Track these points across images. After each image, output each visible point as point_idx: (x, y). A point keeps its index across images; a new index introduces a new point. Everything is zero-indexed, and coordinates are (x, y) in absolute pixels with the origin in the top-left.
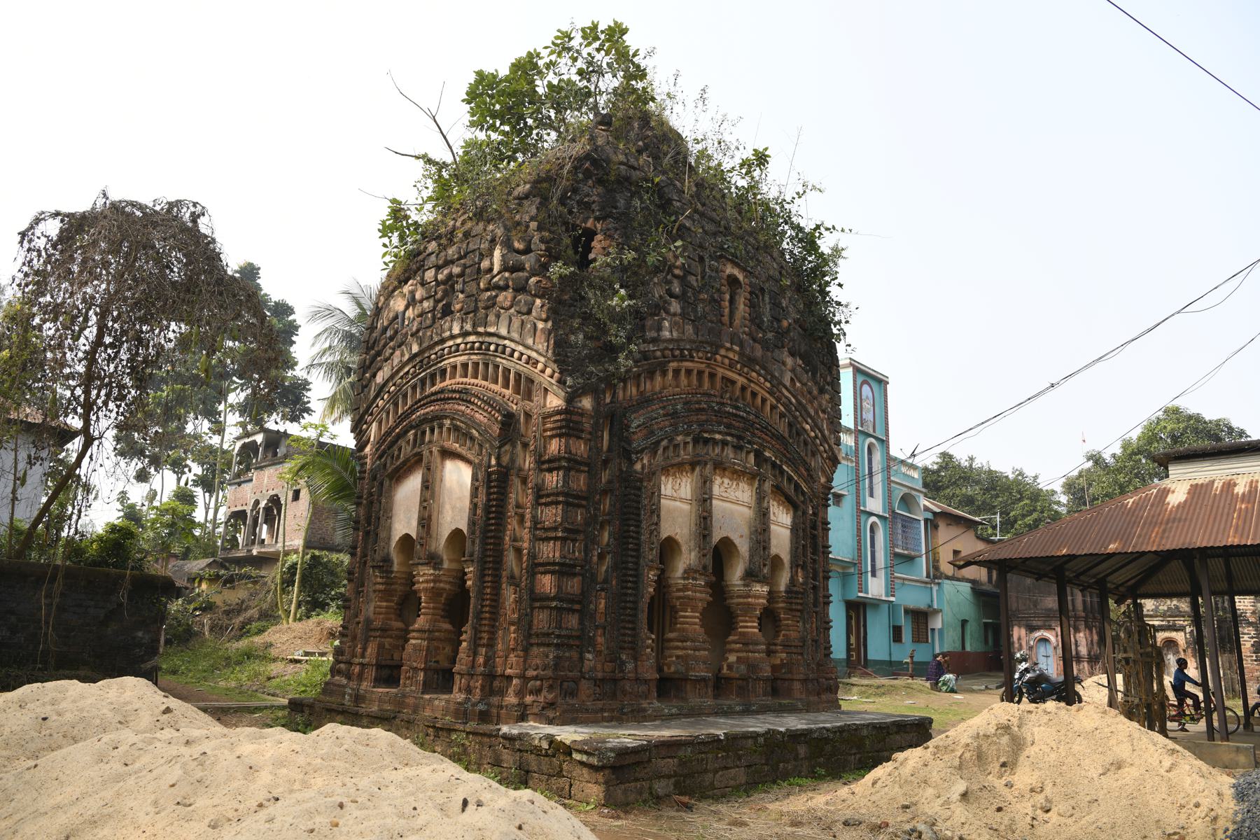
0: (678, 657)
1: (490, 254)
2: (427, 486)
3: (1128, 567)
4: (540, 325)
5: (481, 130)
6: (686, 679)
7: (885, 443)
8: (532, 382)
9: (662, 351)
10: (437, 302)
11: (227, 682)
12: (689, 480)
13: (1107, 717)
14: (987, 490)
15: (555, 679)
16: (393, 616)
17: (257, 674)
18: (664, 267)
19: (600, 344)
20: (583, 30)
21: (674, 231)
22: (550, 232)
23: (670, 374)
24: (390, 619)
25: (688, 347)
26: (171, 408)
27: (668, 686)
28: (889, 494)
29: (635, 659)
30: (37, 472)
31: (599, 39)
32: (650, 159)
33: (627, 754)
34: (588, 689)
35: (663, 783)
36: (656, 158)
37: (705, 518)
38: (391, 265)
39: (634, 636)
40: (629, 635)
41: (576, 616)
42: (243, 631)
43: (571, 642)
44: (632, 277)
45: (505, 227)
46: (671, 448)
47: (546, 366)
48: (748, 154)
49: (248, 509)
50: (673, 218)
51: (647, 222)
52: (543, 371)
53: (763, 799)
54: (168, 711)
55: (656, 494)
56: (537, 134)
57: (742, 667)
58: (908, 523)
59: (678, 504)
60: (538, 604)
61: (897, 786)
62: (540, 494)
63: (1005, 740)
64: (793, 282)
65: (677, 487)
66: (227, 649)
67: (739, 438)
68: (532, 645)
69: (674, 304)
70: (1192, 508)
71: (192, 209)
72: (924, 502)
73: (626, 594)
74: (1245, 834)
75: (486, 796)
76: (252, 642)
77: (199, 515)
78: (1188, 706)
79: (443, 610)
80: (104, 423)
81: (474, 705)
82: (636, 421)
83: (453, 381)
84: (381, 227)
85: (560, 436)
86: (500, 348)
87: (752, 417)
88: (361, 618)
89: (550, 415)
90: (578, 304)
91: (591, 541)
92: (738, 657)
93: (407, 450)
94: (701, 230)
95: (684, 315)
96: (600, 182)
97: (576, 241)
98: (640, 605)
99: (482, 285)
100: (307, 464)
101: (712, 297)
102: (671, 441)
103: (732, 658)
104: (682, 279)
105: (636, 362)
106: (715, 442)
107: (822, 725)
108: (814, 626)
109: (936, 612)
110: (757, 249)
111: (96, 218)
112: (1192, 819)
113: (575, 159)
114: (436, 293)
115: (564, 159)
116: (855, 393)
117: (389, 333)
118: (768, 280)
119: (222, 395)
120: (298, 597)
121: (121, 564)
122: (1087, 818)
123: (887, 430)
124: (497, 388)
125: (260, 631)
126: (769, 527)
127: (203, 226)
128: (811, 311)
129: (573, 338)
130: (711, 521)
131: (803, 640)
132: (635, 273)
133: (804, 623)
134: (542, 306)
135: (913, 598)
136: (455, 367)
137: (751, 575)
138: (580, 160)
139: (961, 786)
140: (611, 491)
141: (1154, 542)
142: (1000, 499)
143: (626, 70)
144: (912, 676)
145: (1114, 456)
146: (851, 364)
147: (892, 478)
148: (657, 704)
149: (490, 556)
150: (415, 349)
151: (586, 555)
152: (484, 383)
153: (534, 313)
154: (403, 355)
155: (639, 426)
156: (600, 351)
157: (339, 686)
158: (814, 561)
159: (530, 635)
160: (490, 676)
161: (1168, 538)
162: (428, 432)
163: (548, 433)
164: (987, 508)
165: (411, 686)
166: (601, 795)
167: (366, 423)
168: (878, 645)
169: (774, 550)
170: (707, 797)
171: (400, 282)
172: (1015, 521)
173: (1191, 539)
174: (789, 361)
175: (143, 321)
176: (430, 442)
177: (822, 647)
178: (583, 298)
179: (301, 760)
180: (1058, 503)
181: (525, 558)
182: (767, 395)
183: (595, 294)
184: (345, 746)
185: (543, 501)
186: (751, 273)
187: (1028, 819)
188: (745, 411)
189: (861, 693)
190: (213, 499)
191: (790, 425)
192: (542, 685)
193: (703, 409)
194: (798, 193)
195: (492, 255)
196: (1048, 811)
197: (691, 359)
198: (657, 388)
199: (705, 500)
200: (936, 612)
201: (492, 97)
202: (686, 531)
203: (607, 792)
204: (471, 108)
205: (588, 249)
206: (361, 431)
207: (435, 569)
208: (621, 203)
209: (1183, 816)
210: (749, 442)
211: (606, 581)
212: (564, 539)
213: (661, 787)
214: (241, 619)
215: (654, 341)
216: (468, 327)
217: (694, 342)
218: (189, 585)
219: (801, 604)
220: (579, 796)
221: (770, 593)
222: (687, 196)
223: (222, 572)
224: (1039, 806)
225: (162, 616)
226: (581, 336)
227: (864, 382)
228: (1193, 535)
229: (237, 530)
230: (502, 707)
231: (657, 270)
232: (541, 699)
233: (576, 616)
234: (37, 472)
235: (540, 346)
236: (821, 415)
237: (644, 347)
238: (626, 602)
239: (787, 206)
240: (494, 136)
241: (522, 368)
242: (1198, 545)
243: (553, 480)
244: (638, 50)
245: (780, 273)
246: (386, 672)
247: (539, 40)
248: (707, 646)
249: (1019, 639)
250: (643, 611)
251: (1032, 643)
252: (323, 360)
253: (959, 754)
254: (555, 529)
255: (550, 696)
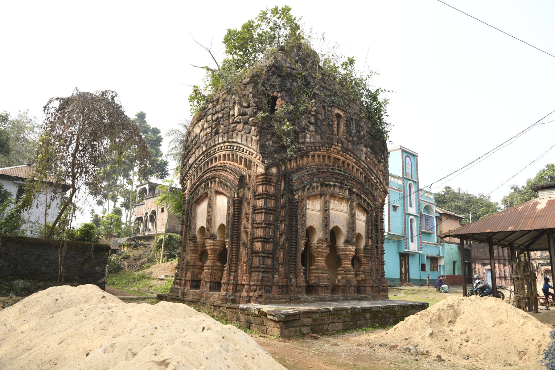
0: (315, 277)
1: (233, 108)
2: (210, 206)
3: (523, 237)
4: (254, 138)
5: (231, 54)
6: (318, 286)
7: (416, 183)
8: (251, 162)
9: (307, 147)
10: (213, 129)
11: (134, 288)
12: (319, 202)
13: (497, 302)
14: (467, 203)
15: (262, 286)
16: (197, 260)
17: (146, 285)
18: (307, 111)
19: (279, 145)
20: (272, 10)
21: (312, 96)
22: (258, 98)
23: (310, 157)
24: (197, 262)
25: (318, 145)
26: (110, 175)
27: (310, 289)
28: (419, 205)
29: (296, 277)
30: (54, 203)
31: (279, 13)
32: (301, 65)
33: (289, 316)
34: (276, 289)
35: (306, 328)
36: (304, 64)
37: (326, 218)
38: (194, 114)
39: (295, 268)
40: (293, 268)
41: (271, 259)
42: (141, 267)
43: (269, 270)
44: (293, 117)
45: (239, 97)
46: (311, 189)
47: (256, 155)
48: (346, 60)
49: (143, 216)
50: (311, 90)
51: (300, 92)
52: (255, 158)
53: (349, 336)
54: (103, 297)
55: (304, 208)
56: (254, 55)
57: (344, 281)
58: (428, 218)
59: (314, 212)
60: (254, 255)
61: (404, 330)
62: (255, 209)
63: (451, 311)
64: (366, 115)
65: (314, 205)
66: (134, 275)
67: (341, 183)
68: (252, 271)
69: (311, 127)
70: (547, 211)
71: (112, 94)
72: (435, 209)
73: (292, 250)
74: (552, 352)
75: (212, 327)
76: (144, 272)
77: (124, 219)
78: (550, 299)
79: (217, 257)
80: (80, 183)
81: (230, 296)
82: (295, 177)
83: (220, 162)
84: (189, 98)
85: (263, 184)
86: (238, 148)
87: (347, 174)
88: (185, 261)
89: (259, 176)
90: (270, 129)
91: (277, 228)
92: (342, 277)
93: (201, 191)
94: (323, 95)
95: (316, 131)
96: (279, 76)
97: (269, 101)
98: (298, 255)
99: (230, 122)
100: (166, 197)
101: (328, 123)
102: (311, 185)
103: (340, 277)
104: (315, 116)
105: (295, 152)
106: (331, 186)
107: (377, 306)
108: (377, 263)
109: (441, 258)
110: (350, 101)
111: (73, 99)
112: (530, 346)
113: (268, 66)
114: (212, 125)
115: (263, 66)
116: (403, 161)
117: (194, 142)
118: (354, 115)
119: (131, 168)
120: (163, 253)
121: (90, 240)
122: (484, 344)
123: (418, 177)
124: (237, 165)
125: (148, 267)
126: (355, 221)
127: (116, 100)
128: (374, 128)
129: (267, 143)
130: (329, 219)
131: (371, 270)
132: (295, 115)
133: (372, 263)
134: (255, 130)
135: (432, 252)
136: (220, 156)
137: (347, 242)
138: (270, 67)
139: (430, 331)
140: (285, 207)
141: (529, 226)
142: (473, 207)
143: (291, 26)
144: (428, 286)
145: (523, 187)
146: (401, 148)
147: (420, 198)
148: (305, 296)
149: (235, 235)
150: (204, 149)
151: (275, 234)
152: (232, 163)
153: (251, 133)
154: (199, 151)
155: (297, 179)
156: (279, 148)
157: (177, 289)
158: (376, 236)
159: (252, 268)
160: (236, 285)
161: (535, 224)
162: (210, 184)
163: (258, 183)
164: (466, 211)
165: (205, 288)
166: (279, 333)
167: (185, 180)
168: (414, 272)
169: (358, 231)
170: (326, 335)
171: (198, 121)
172: (480, 217)
173: (546, 224)
174: (364, 150)
175: (94, 140)
176: (211, 188)
177: (380, 272)
178: (272, 126)
179: (149, 314)
180: (499, 208)
181: (249, 236)
182: (354, 165)
183: (277, 124)
184: (167, 310)
185: (256, 212)
186: (346, 112)
187: (458, 345)
188: (344, 172)
189: (405, 293)
190: (129, 212)
191: (365, 177)
192: (256, 288)
193: (325, 172)
194: (368, 76)
195: (234, 109)
196: (467, 341)
197: (320, 150)
198: (305, 163)
199: (326, 210)
200: (441, 258)
201: (234, 40)
202: (318, 223)
203: (281, 331)
204: (226, 45)
205: (275, 105)
206: (184, 184)
207: (213, 241)
208: (288, 84)
209: (527, 344)
210: (346, 185)
211: (283, 245)
212: (265, 228)
213: (304, 330)
214: (140, 262)
215: (303, 143)
216: (225, 139)
217: (321, 143)
218: (119, 248)
219: (370, 254)
220: (270, 333)
221: (356, 250)
222: (317, 80)
223: (132, 243)
224: (464, 339)
225: (106, 261)
226: (271, 142)
227: (407, 156)
228: (546, 222)
229: (139, 225)
230: (240, 297)
231: (304, 113)
232: (256, 294)
233: (271, 259)
234: (54, 203)
235: (254, 147)
236: (379, 173)
237: (298, 146)
238: (292, 254)
239: (364, 82)
240: (236, 57)
241: (247, 156)
242: (548, 227)
243: (260, 203)
244: (296, 17)
245: (360, 111)
246: (195, 283)
247: (253, 16)
248: (328, 272)
249: (479, 269)
250: (299, 258)
251: (484, 271)
252: (173, 152)
253: (430, 317)
254: (261, 223)
255: (260, 293)
